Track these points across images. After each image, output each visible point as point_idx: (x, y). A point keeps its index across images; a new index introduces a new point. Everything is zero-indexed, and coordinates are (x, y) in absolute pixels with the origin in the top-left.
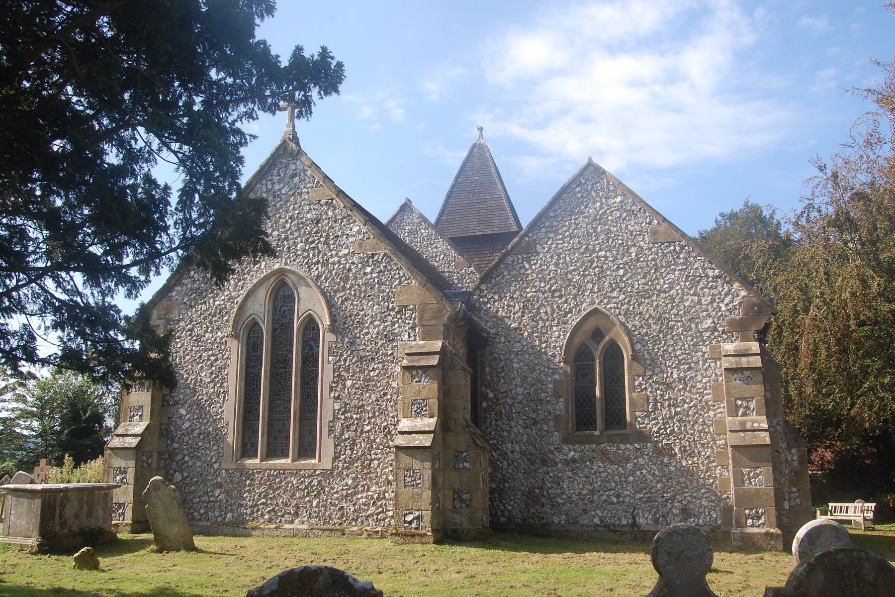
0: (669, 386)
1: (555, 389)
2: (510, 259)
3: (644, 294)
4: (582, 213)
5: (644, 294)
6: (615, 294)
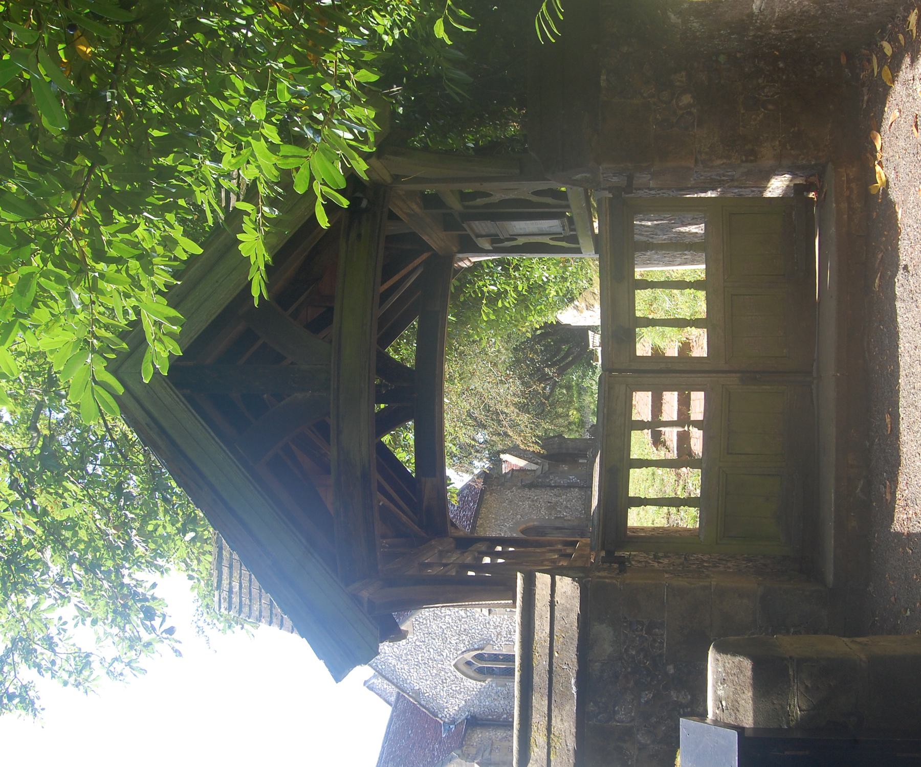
0: (499, 634)
1: (501, 686)
2: (422, 702)
3: (445, 640)
4: (394, 666)
5: (445, 640)
6: (445, 654)
